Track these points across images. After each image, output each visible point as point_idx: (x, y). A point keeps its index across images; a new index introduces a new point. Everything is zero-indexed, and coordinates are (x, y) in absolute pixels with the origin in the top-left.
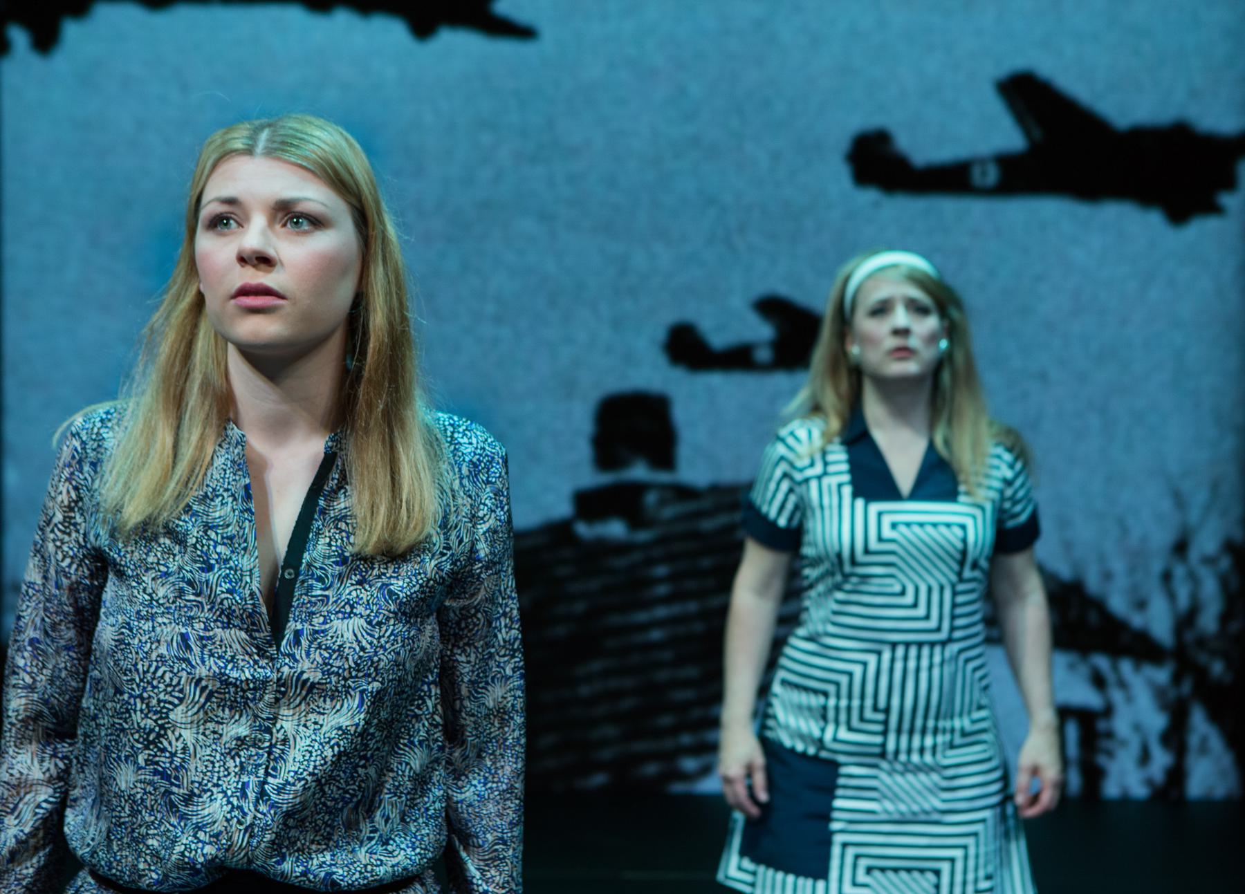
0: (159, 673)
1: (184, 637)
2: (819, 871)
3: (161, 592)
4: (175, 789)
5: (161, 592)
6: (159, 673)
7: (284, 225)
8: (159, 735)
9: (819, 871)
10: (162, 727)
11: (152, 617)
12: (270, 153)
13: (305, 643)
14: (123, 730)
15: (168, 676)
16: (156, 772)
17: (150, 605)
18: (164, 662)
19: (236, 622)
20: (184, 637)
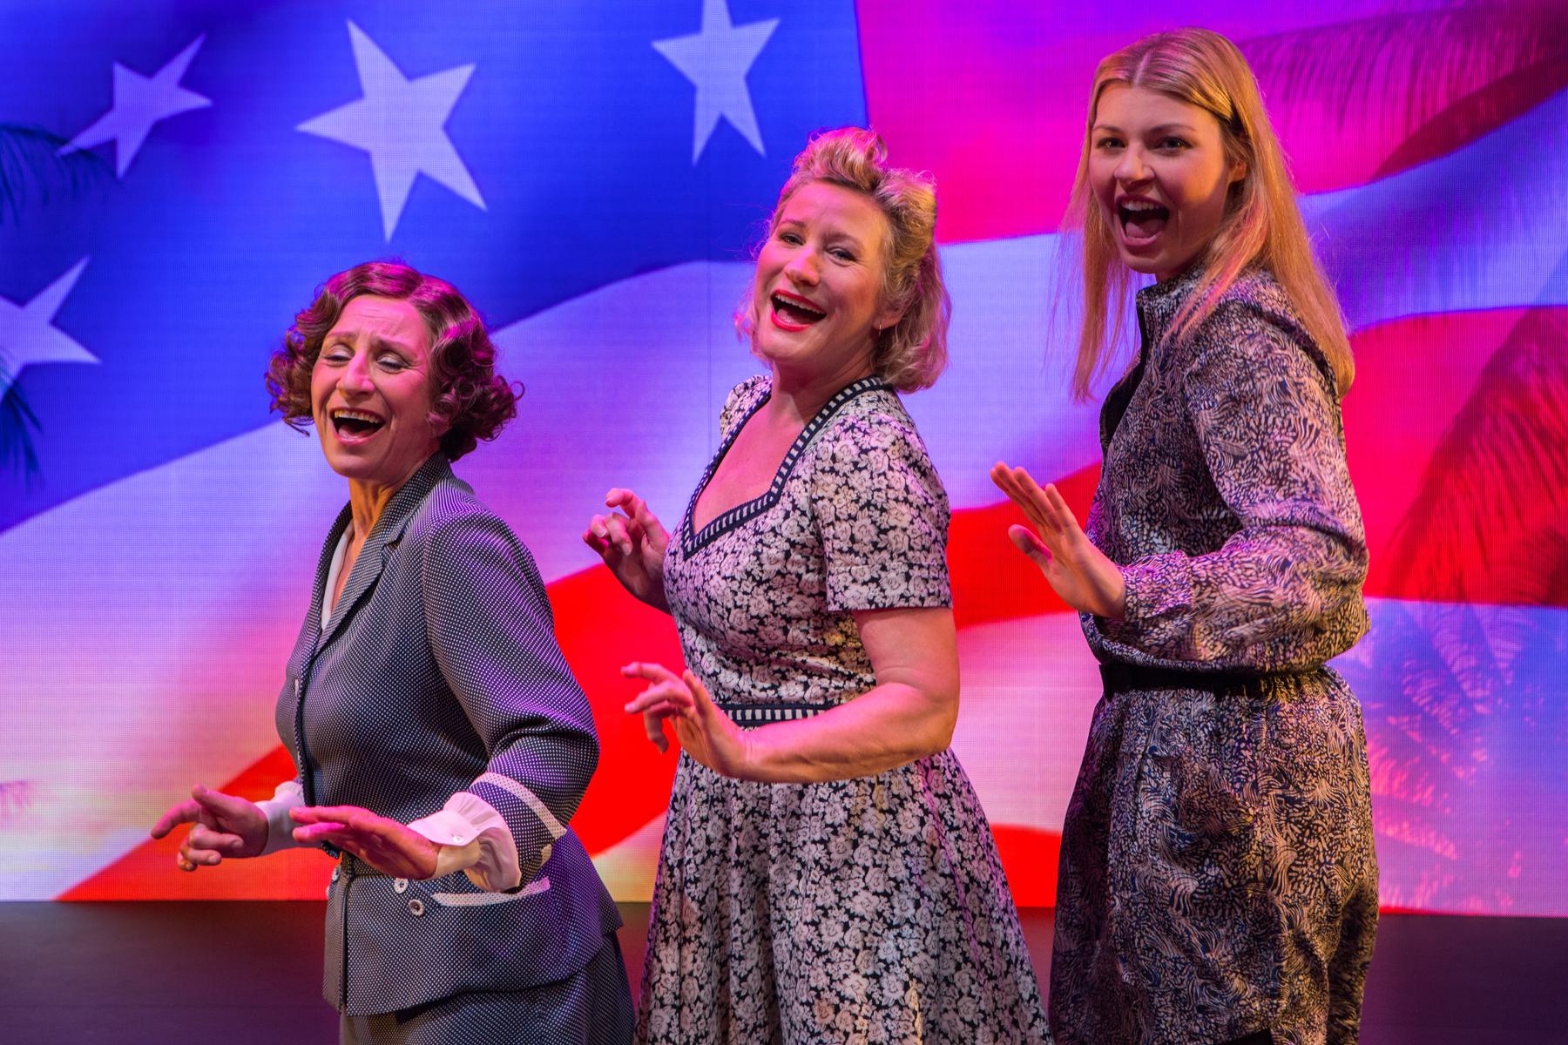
0: (1270, 421)
1: (1286, 563)
2: (421, 178)
3: (1251, 352)
4: (1280, 792)
5: (1251, 352)
6: (1270, 421)
7: (1001, 478)
8: (1303, 834)
9: (421, 178)
10: (1302, 843)
11: (1251, 376)
12: (1145, 83)
13: (1287, 576)
14: (1333, 830)
15: (1278, 421)
16: (1299, 802)
17: (1246, 366)
18: (1271, 411)
19: (1170, 964)
20: (1286, 563)
